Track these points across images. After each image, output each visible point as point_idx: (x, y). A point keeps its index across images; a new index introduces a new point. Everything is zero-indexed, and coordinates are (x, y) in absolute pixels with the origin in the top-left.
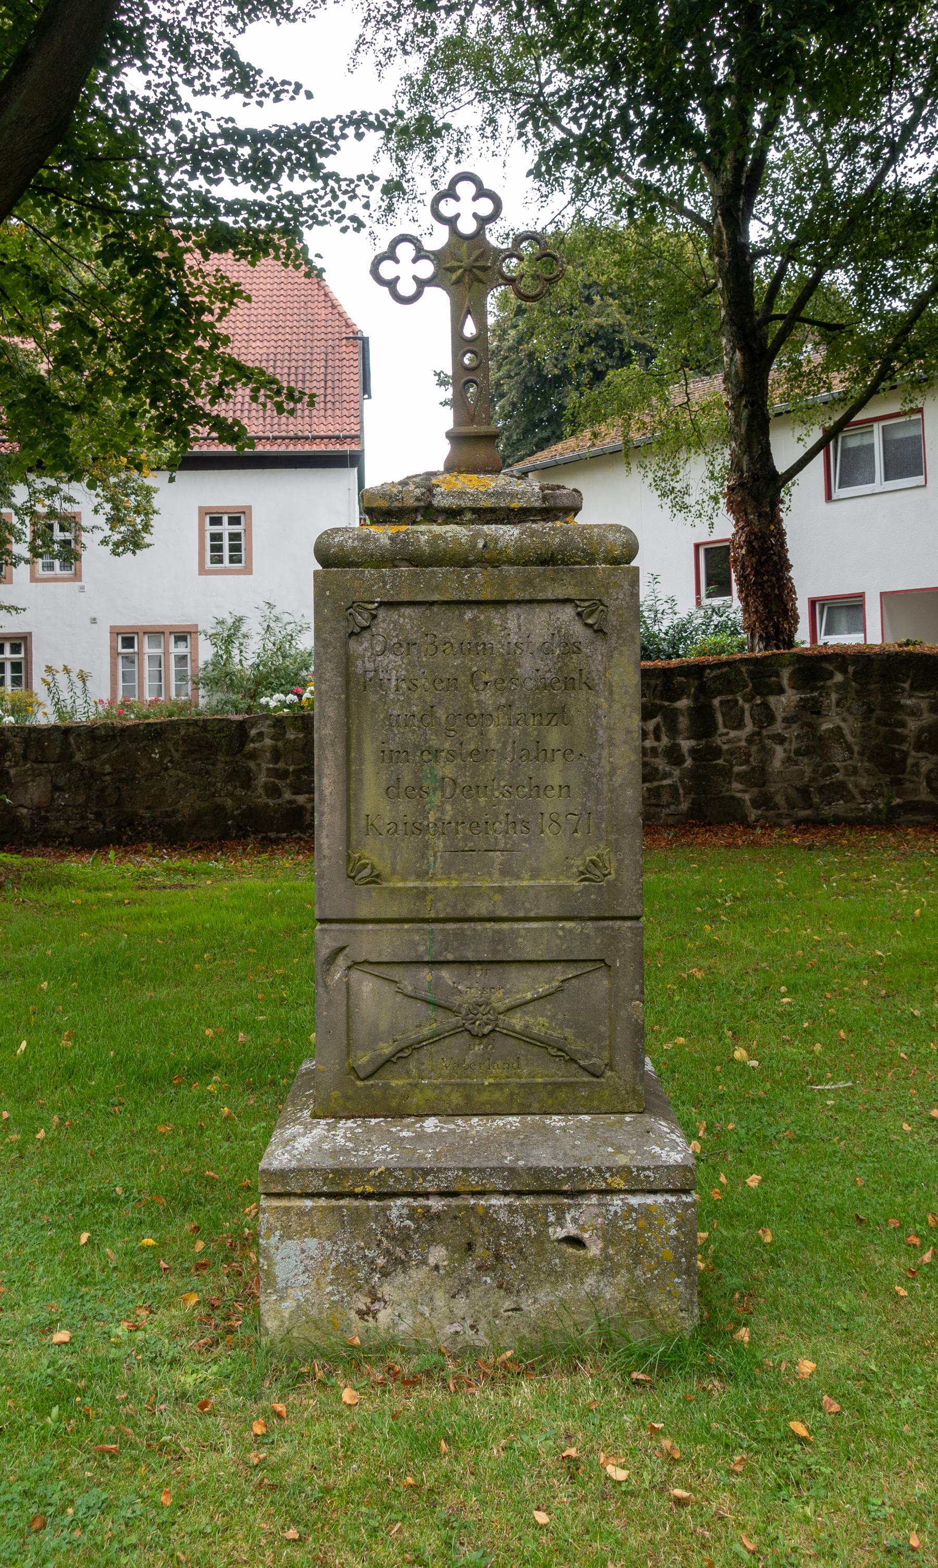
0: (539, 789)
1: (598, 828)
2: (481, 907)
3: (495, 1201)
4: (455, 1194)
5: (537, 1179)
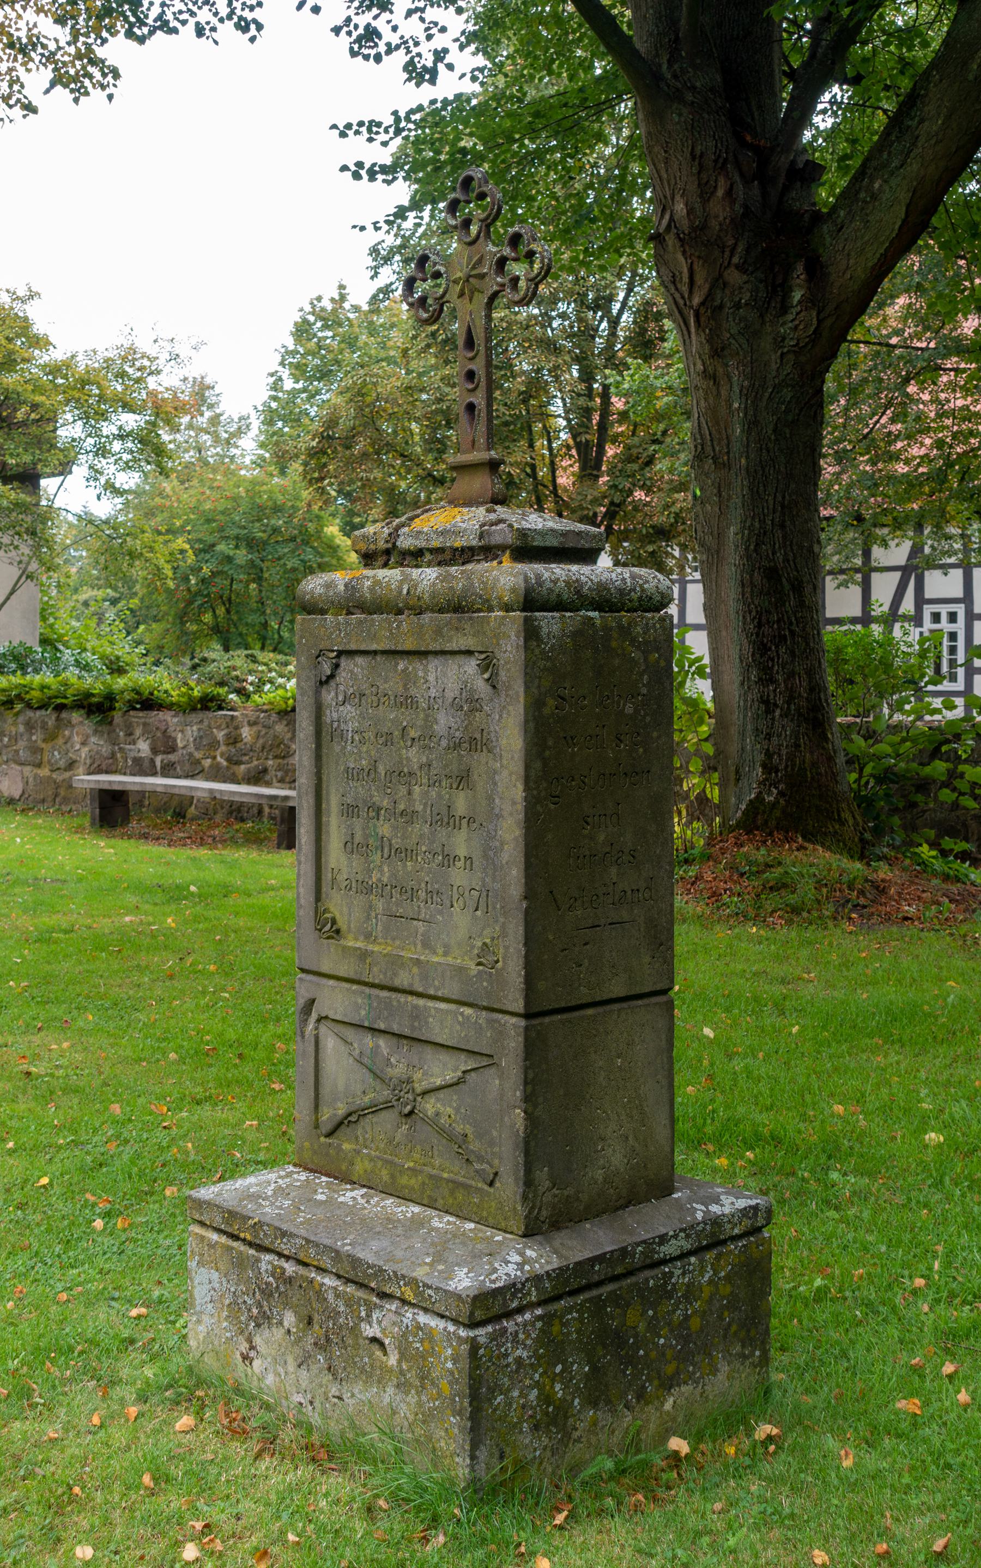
0: (449, 859)
1: (494, 908)
2: (403, 979)
3: (329, 1281)
4: (306, 1265)
5: (354, 1269)
